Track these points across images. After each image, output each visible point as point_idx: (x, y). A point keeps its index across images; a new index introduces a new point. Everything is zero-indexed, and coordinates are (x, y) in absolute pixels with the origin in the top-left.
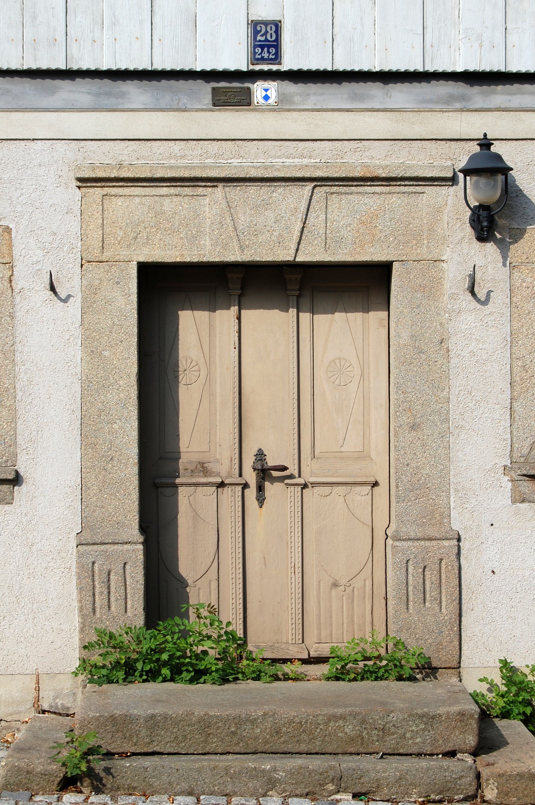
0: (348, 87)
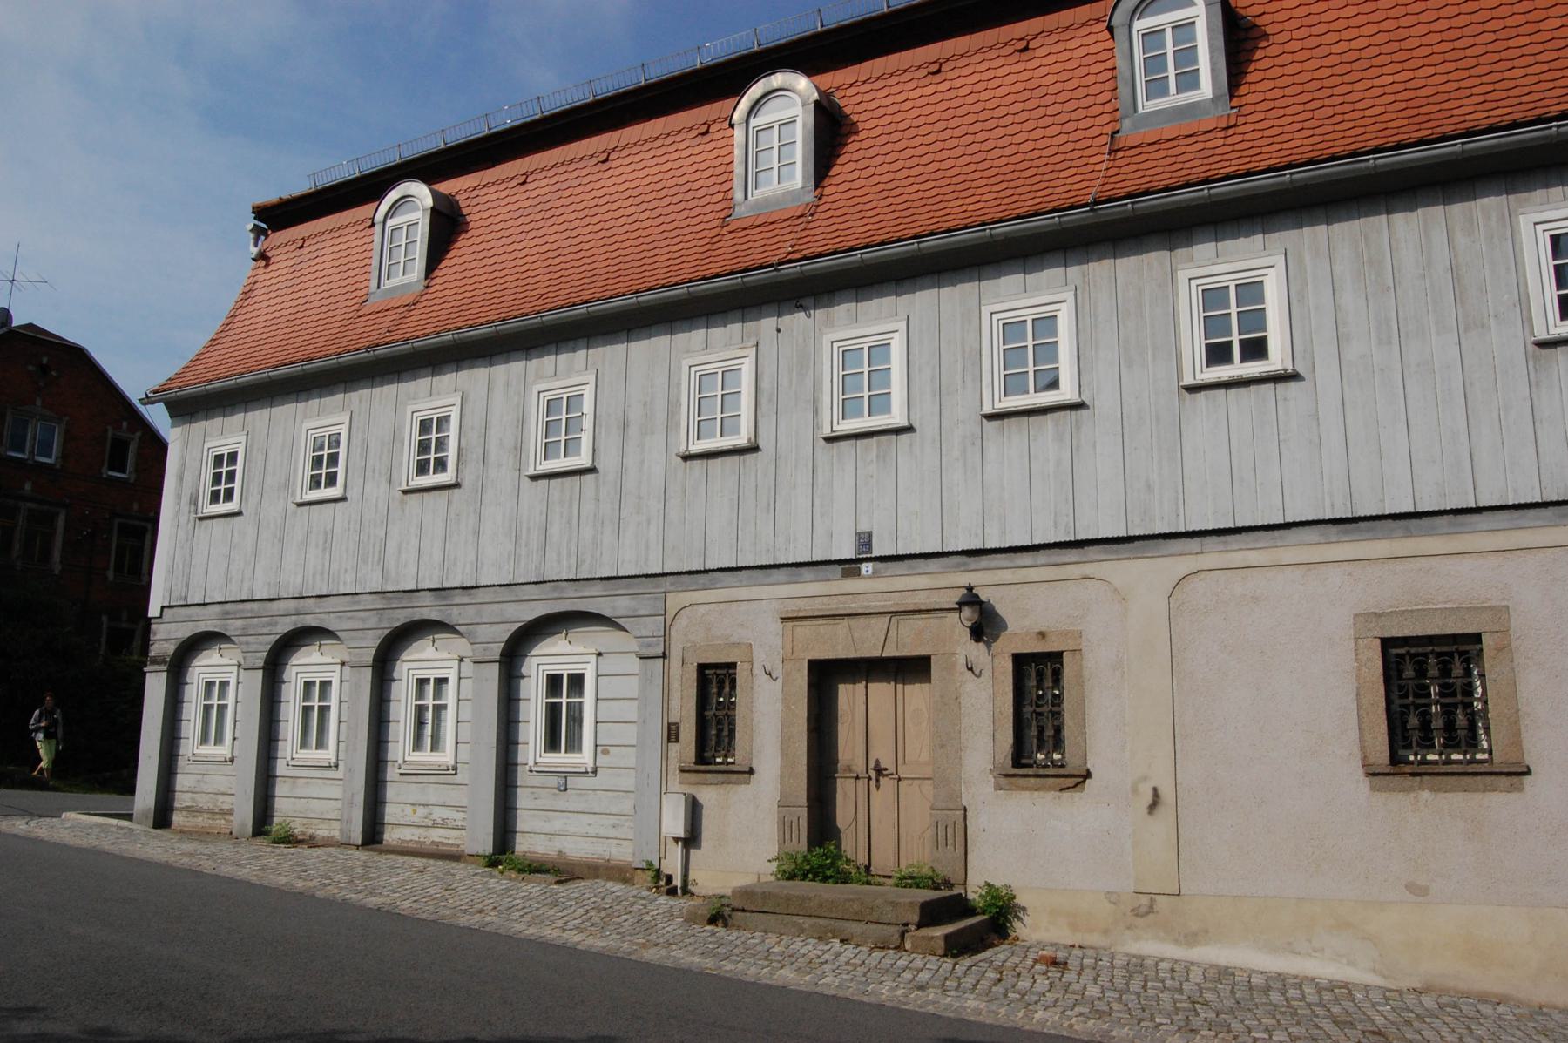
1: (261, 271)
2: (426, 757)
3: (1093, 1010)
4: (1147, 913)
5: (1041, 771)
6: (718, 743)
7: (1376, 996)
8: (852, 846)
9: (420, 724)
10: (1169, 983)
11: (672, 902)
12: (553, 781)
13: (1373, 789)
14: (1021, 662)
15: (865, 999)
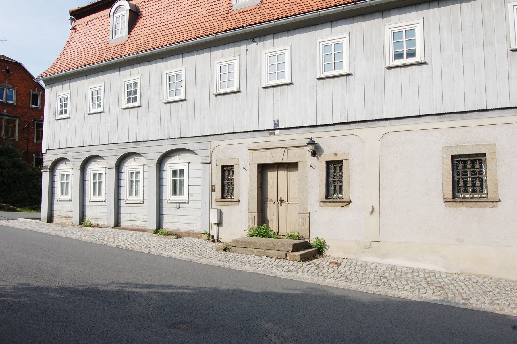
0: (291, 130)
1: (74, 34)
2: (133, 198)
3: (346, 279)
4: (369, 248)
5: (335, 201)
6: (228, 192)
7: (443, 275)
8: (272, 226)
9: (131, 187)
10: (374, 270)
11: (213, 244)
12: (175, 205)
13: (446, 206)
14: (328, 164)
15: (271, 275)
